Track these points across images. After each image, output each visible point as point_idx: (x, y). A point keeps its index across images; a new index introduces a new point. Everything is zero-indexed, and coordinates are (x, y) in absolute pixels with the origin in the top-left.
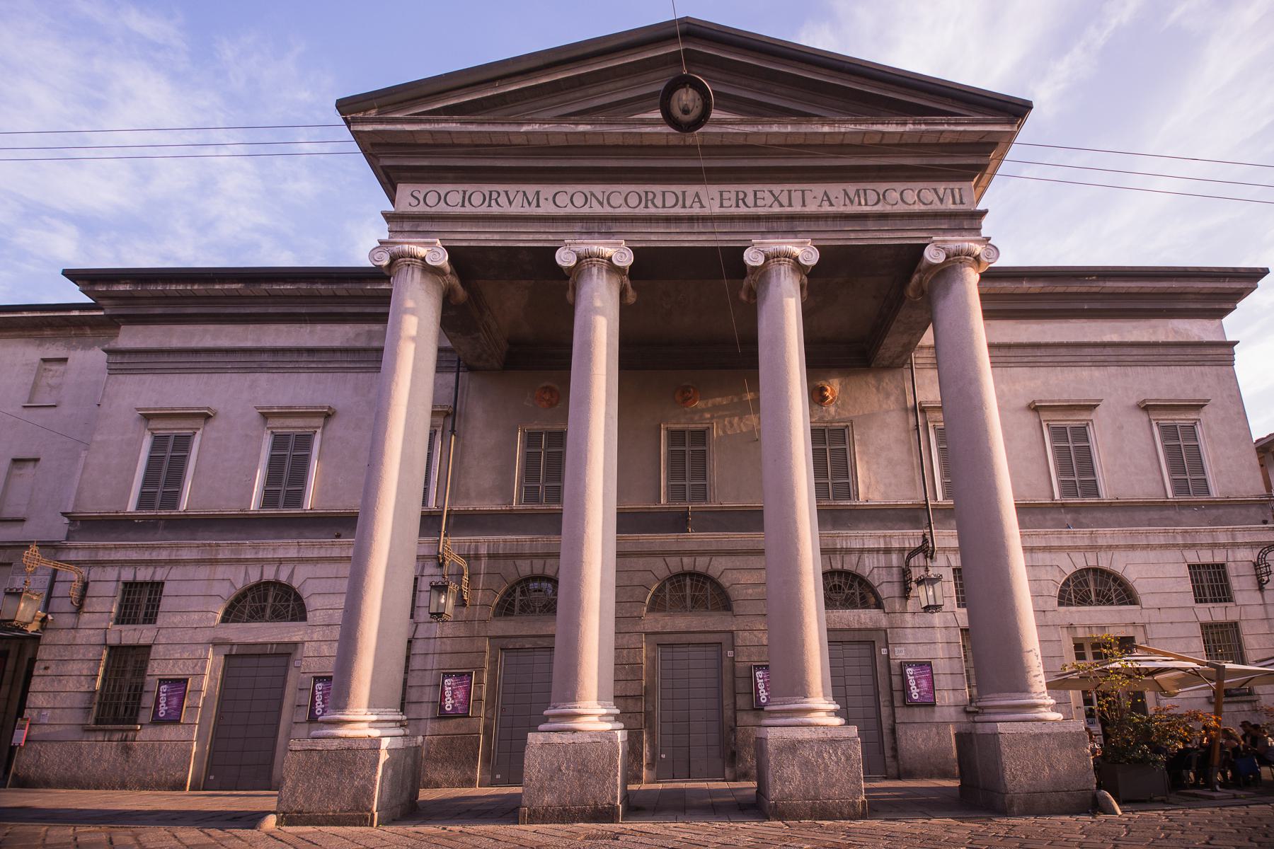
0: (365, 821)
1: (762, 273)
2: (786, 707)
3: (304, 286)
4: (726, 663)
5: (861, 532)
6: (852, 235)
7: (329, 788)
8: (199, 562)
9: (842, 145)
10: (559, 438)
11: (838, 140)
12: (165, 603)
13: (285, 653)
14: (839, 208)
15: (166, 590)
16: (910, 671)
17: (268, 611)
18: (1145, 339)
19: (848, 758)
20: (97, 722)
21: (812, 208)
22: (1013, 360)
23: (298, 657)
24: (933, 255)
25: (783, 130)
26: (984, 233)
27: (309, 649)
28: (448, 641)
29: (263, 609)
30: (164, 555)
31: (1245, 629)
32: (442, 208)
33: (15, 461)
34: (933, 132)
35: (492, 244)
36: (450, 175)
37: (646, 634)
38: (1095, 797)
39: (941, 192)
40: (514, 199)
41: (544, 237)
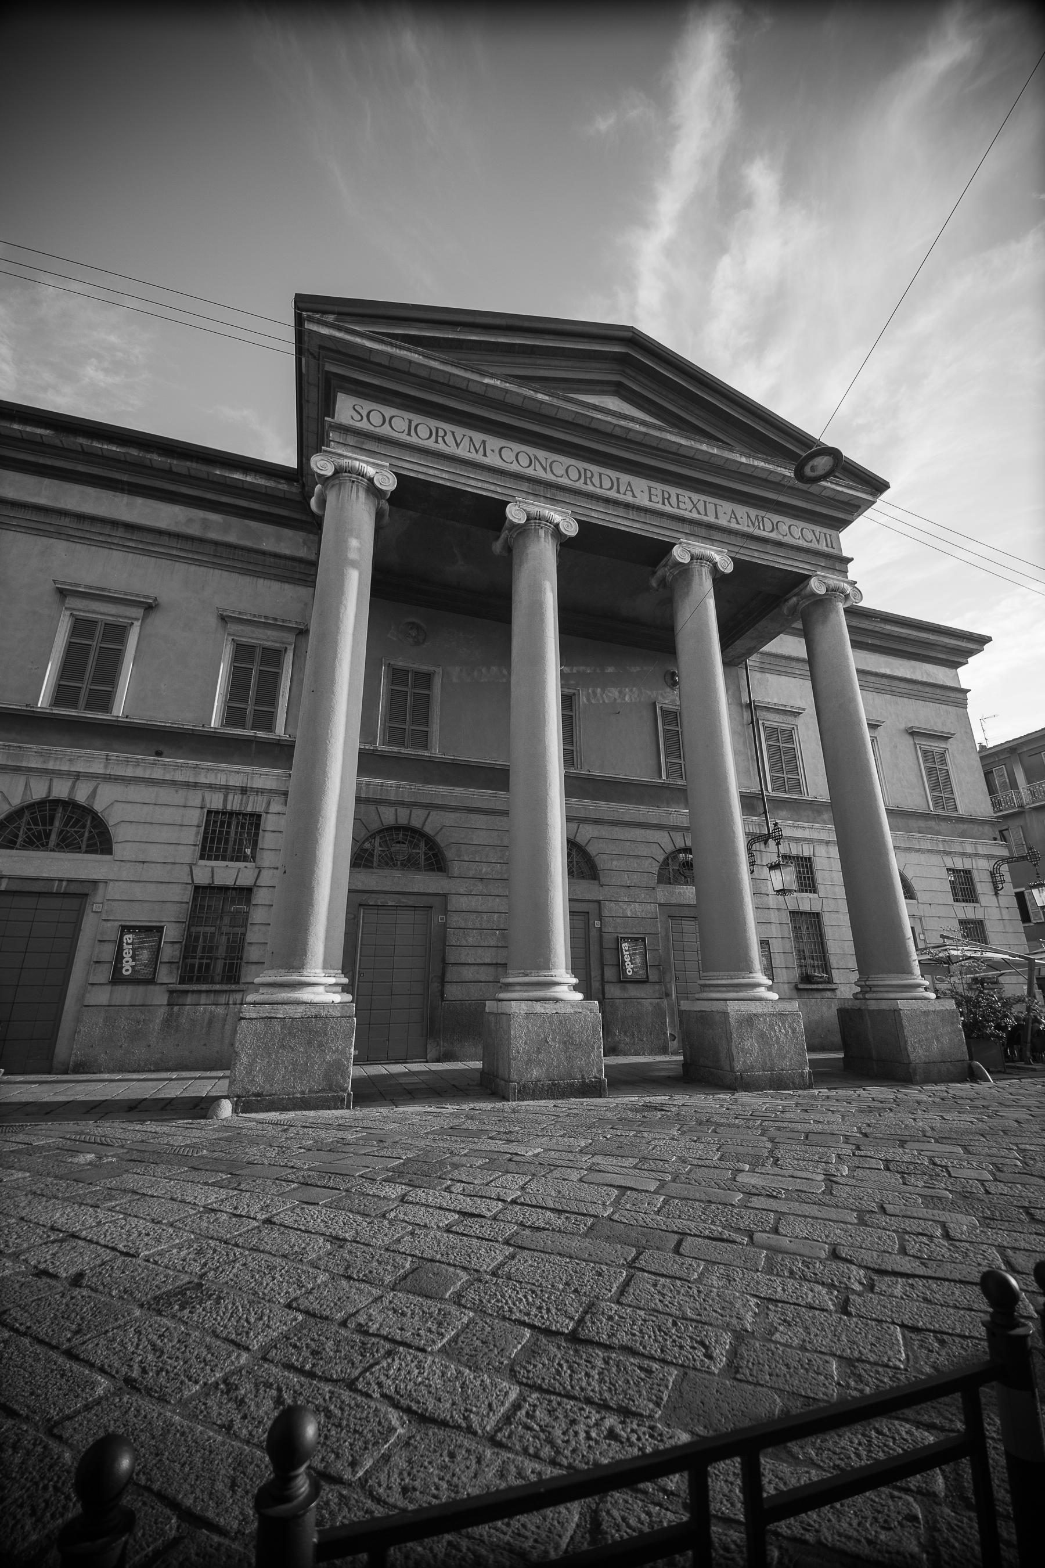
1: (684, 571)
2: (736, 981)
3: (134, 452)
4: (594, 933)
6: (756, 554)
7: (294, 1064)
9: (750, 476)
13: (79, 895)
14: (744, 528)
16: (625, 946)
17: (53, 837)
18: (908, 676)
19: (794, 1031)
21: (723, 522)
23: (99, 898)
24: (680, 554)
26: (851, 576)
27: (114, 891)
29: (48, 836)
31: (987, 924)
32: (385, 430)
35: (441, 482)
36: (398, 400)
38: (970, 1067)
39: (817, 534)
41: (492, 488)
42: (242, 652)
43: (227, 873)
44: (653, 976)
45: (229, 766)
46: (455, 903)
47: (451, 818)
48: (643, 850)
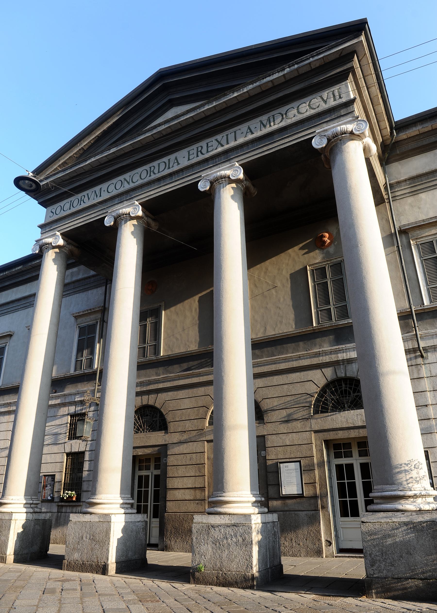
10: (338, 268)
11: (247, 96)
32: (64, 214)
40: (160, 167)
41: (101, 212)
42: (82, 331)
45: (348, 345)
47: (163, 397)
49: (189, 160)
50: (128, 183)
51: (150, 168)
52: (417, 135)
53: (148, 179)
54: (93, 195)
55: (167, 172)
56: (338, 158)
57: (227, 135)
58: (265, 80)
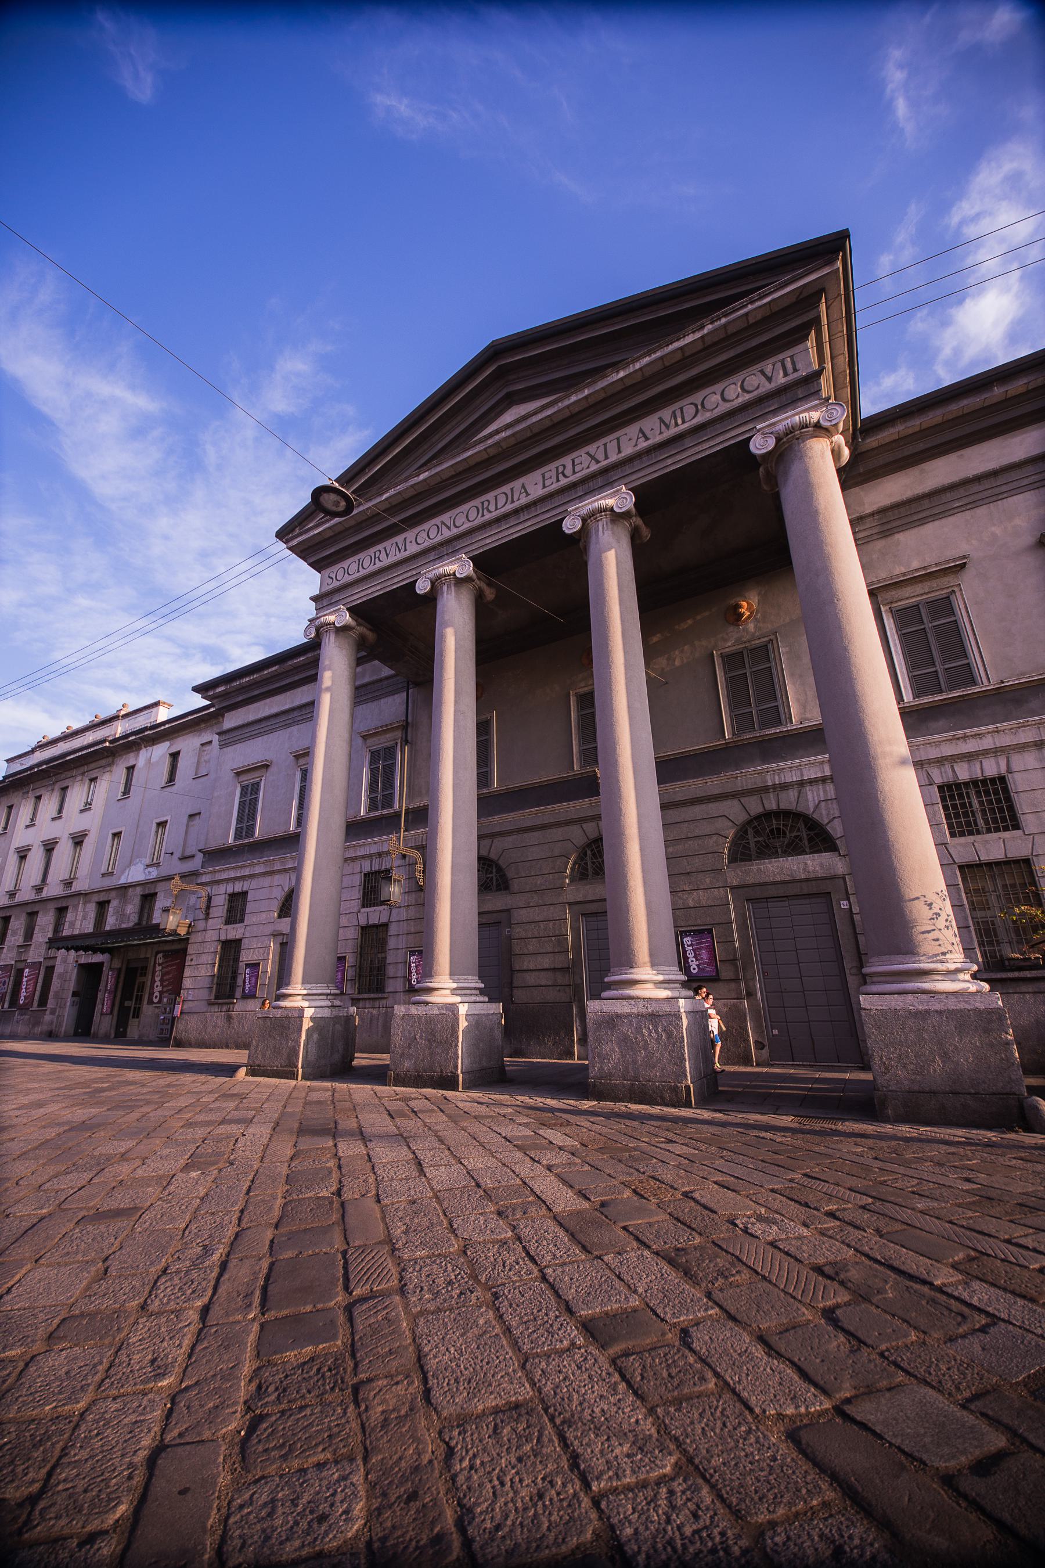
0: (292, 1076)
5: (796, 762)
6: (669, 461)
7: (275, 1047)
8: (265, 874)
11: (639, 377)
12: (250, 907)
15: (250, 897)
20: (217, 997)
21: (628, 451)
22: (1004, 488)
25: (580, 396)
28: (412, 923)
30: (246, 872)
32: (348, 579)
33: (191, 816)
34: (734, 320)
37: (570, 904)
40: (498, 501)
41: (409, 574)
42: (375, 756)
43: (376, 915)
44: (726, 973)
46: (522, 915)
47: (508, 842)
48: (706, 828)
49: (544, 487)
50: (449, 528)
51: (483, 503)
52: (895, 441)
53: (480, 521)
54: (393, 549)
55: (509, 507)
56: (795, 469)
57: (605, 445)
58: (671, 348)
